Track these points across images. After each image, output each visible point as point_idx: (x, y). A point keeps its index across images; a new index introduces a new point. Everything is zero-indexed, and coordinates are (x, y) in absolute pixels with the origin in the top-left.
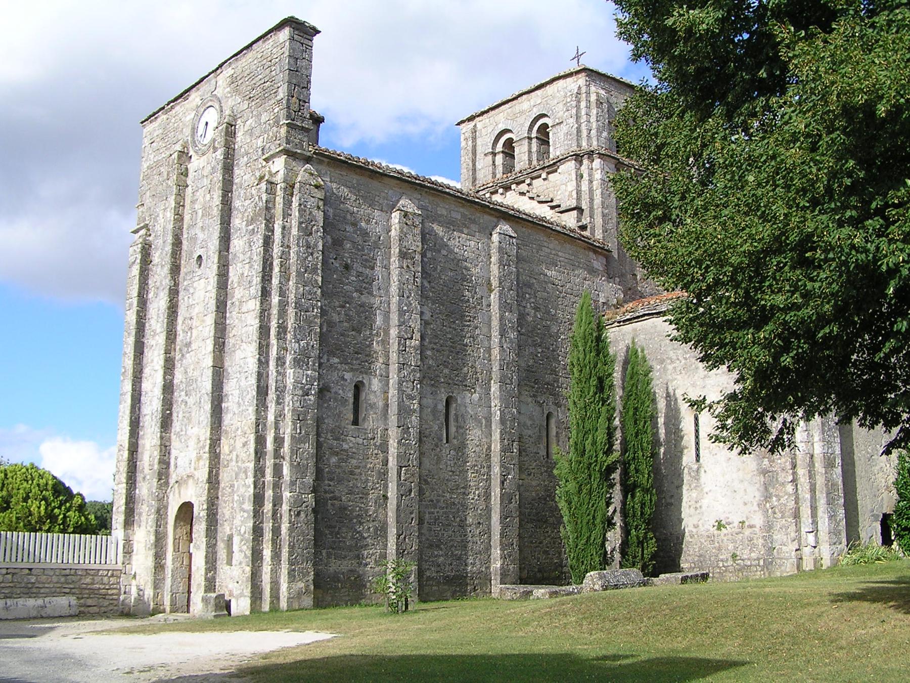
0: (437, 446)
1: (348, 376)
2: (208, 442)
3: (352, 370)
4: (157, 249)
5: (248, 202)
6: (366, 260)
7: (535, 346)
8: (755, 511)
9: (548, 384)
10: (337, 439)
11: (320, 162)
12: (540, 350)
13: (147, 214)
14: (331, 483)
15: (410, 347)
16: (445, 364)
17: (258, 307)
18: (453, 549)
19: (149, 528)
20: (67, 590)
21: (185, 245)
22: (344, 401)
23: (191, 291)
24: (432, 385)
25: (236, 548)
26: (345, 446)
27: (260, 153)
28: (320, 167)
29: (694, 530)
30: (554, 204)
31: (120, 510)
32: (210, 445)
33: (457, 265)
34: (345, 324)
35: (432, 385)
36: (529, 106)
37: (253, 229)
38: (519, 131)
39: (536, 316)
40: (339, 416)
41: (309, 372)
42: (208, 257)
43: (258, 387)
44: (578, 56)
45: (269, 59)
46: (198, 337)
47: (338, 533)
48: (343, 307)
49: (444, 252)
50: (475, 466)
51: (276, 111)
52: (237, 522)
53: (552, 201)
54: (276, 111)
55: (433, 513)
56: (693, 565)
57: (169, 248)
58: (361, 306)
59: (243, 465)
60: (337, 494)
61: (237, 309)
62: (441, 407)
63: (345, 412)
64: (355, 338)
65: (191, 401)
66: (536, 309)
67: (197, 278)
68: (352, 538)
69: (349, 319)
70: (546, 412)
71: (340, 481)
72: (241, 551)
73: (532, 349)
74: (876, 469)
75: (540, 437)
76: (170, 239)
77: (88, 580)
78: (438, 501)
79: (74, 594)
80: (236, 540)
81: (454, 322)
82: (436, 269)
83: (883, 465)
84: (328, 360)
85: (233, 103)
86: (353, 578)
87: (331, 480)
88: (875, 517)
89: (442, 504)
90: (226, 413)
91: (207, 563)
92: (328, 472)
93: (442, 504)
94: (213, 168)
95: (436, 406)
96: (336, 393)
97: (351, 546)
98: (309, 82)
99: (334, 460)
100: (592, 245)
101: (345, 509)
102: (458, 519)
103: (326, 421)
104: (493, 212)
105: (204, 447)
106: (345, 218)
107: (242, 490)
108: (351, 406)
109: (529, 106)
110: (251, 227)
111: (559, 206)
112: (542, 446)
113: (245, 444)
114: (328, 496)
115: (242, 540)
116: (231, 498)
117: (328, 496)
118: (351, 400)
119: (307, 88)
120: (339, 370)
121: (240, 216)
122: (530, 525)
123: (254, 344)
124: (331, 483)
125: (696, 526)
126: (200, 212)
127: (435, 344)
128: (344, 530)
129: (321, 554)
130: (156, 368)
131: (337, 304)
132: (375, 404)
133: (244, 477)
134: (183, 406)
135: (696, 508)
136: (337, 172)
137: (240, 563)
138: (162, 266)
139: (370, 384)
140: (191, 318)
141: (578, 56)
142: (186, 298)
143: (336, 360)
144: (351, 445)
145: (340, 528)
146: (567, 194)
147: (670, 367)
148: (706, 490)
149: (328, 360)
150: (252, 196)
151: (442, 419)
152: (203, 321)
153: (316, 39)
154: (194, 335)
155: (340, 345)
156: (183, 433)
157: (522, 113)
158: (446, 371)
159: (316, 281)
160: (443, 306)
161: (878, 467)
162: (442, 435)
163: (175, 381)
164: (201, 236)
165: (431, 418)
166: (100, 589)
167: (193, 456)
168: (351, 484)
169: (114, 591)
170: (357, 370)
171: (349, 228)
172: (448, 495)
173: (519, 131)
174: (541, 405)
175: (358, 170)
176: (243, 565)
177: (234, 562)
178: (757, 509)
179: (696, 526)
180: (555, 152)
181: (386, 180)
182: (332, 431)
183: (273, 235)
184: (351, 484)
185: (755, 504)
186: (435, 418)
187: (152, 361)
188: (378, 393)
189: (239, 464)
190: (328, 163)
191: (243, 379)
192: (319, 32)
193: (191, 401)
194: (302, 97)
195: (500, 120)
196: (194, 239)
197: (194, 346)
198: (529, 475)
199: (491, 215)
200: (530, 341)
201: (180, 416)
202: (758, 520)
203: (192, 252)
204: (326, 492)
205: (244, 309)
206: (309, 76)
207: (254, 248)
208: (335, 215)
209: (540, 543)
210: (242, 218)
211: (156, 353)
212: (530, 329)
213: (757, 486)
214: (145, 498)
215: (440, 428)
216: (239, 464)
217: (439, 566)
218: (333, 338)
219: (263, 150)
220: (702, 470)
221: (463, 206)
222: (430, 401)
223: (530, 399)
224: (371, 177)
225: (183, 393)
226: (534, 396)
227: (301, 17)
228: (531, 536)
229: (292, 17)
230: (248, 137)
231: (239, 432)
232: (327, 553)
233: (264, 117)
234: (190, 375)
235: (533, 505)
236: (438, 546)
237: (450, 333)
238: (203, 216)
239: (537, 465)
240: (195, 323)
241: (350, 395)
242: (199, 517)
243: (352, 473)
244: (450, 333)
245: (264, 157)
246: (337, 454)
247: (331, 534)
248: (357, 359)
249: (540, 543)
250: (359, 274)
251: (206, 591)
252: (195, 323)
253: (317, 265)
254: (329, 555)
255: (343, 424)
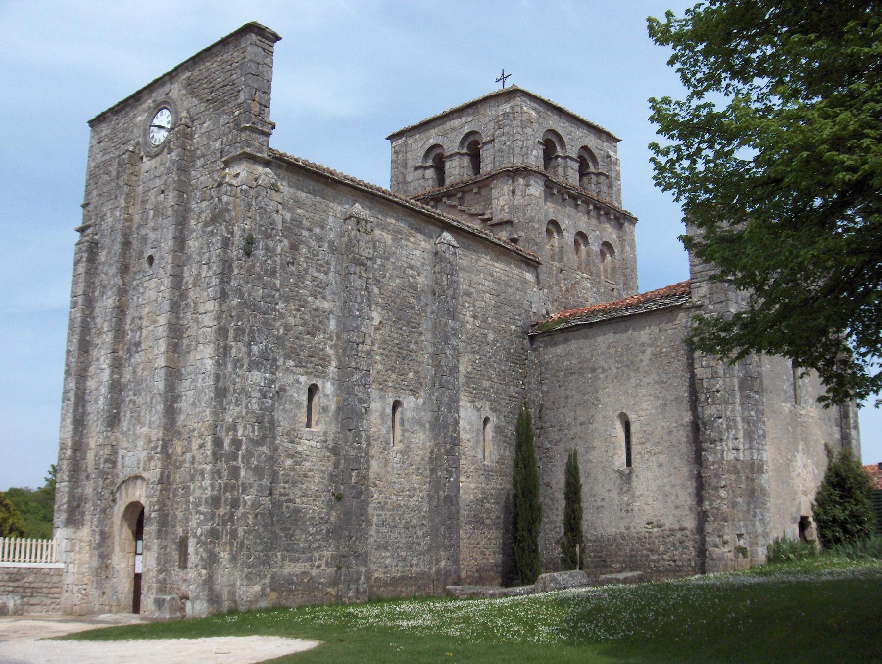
0: (384, 449)
1: (303, 379)
2: (161, 442)
3: (307, 373)
4: (103, 248)
5: (205, 203)
6: (321, 265)
7: (473, 352)
8: (686, 515)
9: (484, 389)
10: (292, 442)
11: (279, 167)
12: (478, 357)
13: (93, 213)
14: (286, 486)
15: (362, 352)
16: (393, 369)
17: (216, 309)
18: (399, 551)
19: (94, 528)
20: (11, 589)
21: (135, 244)
22: (299, 404)
23: (141, 290)
24: (381, 389)
25: (191, 550)
26: (300, 449)
27: (218, 155)
28: (279, 171)
29: (626, 532)
30: (486, 217)
31: (62, 508)
32: (163, 445)
33: (404, 272)
34: (301, 328)
35: (381, 389)
36: (464, 125)
37: (212, 231)
38: (452, 144)
39: (474, 324)
40: (294, 420)
41: (267, 375)
42: (162, 258)
43: (216, 389)
44: (504, 78)
45: (230, 62)
46: (147, 338)
47: (293, 536)
48: (298, 310)
49: (393, 260)
50: (419, 468)
51: (236, 113)
52: (193, 524)
53: (483, 215)
54: (236, 113)
55: (380, 515)
56: (624, 565)
57: (117, 247)
58: (315, 310)
59: (200, 467)
60: (291, 496)
61: (191, 310)
62: (389, 410)
63: (299, 415)
64: (309, 342)
65: (140, 400)
66: (475, 317)
67: (147, 278)
68: (306, 540)
69: (305, 324)
70: (483, 417)
71: (294, 484)
72: (197, 554)
73: (471, 356)
74: (793, 474)
75: (477, 441)
76: (119, 239)
77: (31, 579)
78: (386, 503)
79: (18, 592)
80: (192, 542)
81: (401, 329)
82: (384, 276)
83: (800, 470)
84: (284, 363)
85: (189, 105)
86: (306, 580)
87: (286, 482)
88: (794, 519)
89: (389, 506)
90: (179, 414)
91: (158, 564)
92: (283, 475)
93: (389, 506)
94: (168, 169)
95: (384, 410)
96: (291, 396)
97: (304, 548)
98: (270, 87)
99: (289, 462)
100: (525, 257)
101: (299, 511)
102: (404, 521)
103: (282, 424)
104: (437, 223)
105: (156, 447)
106: (301, 223)
107: (198, 493)
108: (305, 410)
109: (464, 125)
110: (209, 229)
111: (491, 219)
112: (480, 450)
113: (201, 446)
114: (283, 498)
115: (198, 543)
116: (184, 499)
117: (283, 498)
118: (305, 403)
119: (267, 92)
120: (294, 373)
121: (196, 217)
122: (468, 527)
123: (212, 345)
124: (286, 486)
125: (628, 529)
126: (152, 213)
127: (384, 349)
128: (298, 532)
129: (276, 557)
130: (103, 366)
131: (293, 307)
132: (327, 407)
133: (200, 479)
134: (131, 406)
135: (627, 511)
136: (294, 178)
137: (196, 566)
138: (111, 265)
139: (323, 387)
140: (141, 318)
141: (504, 78)
142: (135, 298)
143: (291, 363)
144: (305, 447)
145: (294, 531)
146: (499, 207)
147: (602, 376)
148: (637, 493)
149: (284, 363)
150: (212, 198)
151: (390, 423)
152: (155, 322)
153: (277, 45)
154: (144, 335)
155: (296, 349)
156: (131, 433)
157: (453, 129)
158: (394, 376)
159: (275, 284)
160: (391, 311)
161: (796, 473)
162: (389, 438)
163: (124, 381)
164: (152, 236)
165: (379, 421)
166: (41, 588)
167: (143, 455)
168: (304, 487)
169: (58, 590)
170: (310, 373)
171: (305, 233)
172: (394, 498)
173: (452, 144)
174: (478, 410)
175: (315, 176)
176: (200, 567)
177: (189, 565)
178: (688, 512)
179: (628, 529)
180: (487, 167)
181: (341, 187)
182: (288, 434)
183: (232, 236)
184: (304, 487)
185: (687, 508)
186: (384, 422)
187: (98, 360)
188: (331, 397)
189: (196, 465)
190: (287, 169)
191: (200, 380)
192: (277, 38)
193: (140, 400)
194: (263, 102)
195: (432, 138)
196: (144, 240)
197: (143, 346)
198: (468, 477)
199: (435, 225)
200: (469, 347)
201: (128, 415)
202: (690, 523)
203: (142, 252)
204: (281, 495)
205: (202, 310)
206: (269, 81)
207: (212, 249)
208: (292, 220)
209: (478, 544)
210: (198, 220)
211: (103, 352)
212: (469, 336)
213: (690, 490)
214: (90, 497)
215: (388, 432)
216: (196, 465)
217: (386, 567)
218: (289, 341)
219: (221, 152)
220: (634, 476)
221: (410, 216)
222: (379, 405)
223: (469, 404)
224: (326, 184)
225: (131, 393)
226: (473, 401)
227: (263, 23)
228: (469, 538)
229: (255, 23)
230: (204, 139)
231: (196, 434)
232: (282, 555)
233: (224, 119)
234: (139, 374)
235: (472, 507)
236: (385, 548)
237: (398, 339)
238: (154, 216)
239: (475, 468)
240: (144, 323)
241: (305, 398)
242: (150, 518)
243: (306, 475)
244: (398, 339)
245: (223, 159)
246: (292, 456)
247: (286, 535)
248: (311, 362)
249: (478, 544)
250: (314, 279)
251: (157, 593)
252: (144, 323)
253: (275, 268)
254: (283, 558)
255: (297, 426)
